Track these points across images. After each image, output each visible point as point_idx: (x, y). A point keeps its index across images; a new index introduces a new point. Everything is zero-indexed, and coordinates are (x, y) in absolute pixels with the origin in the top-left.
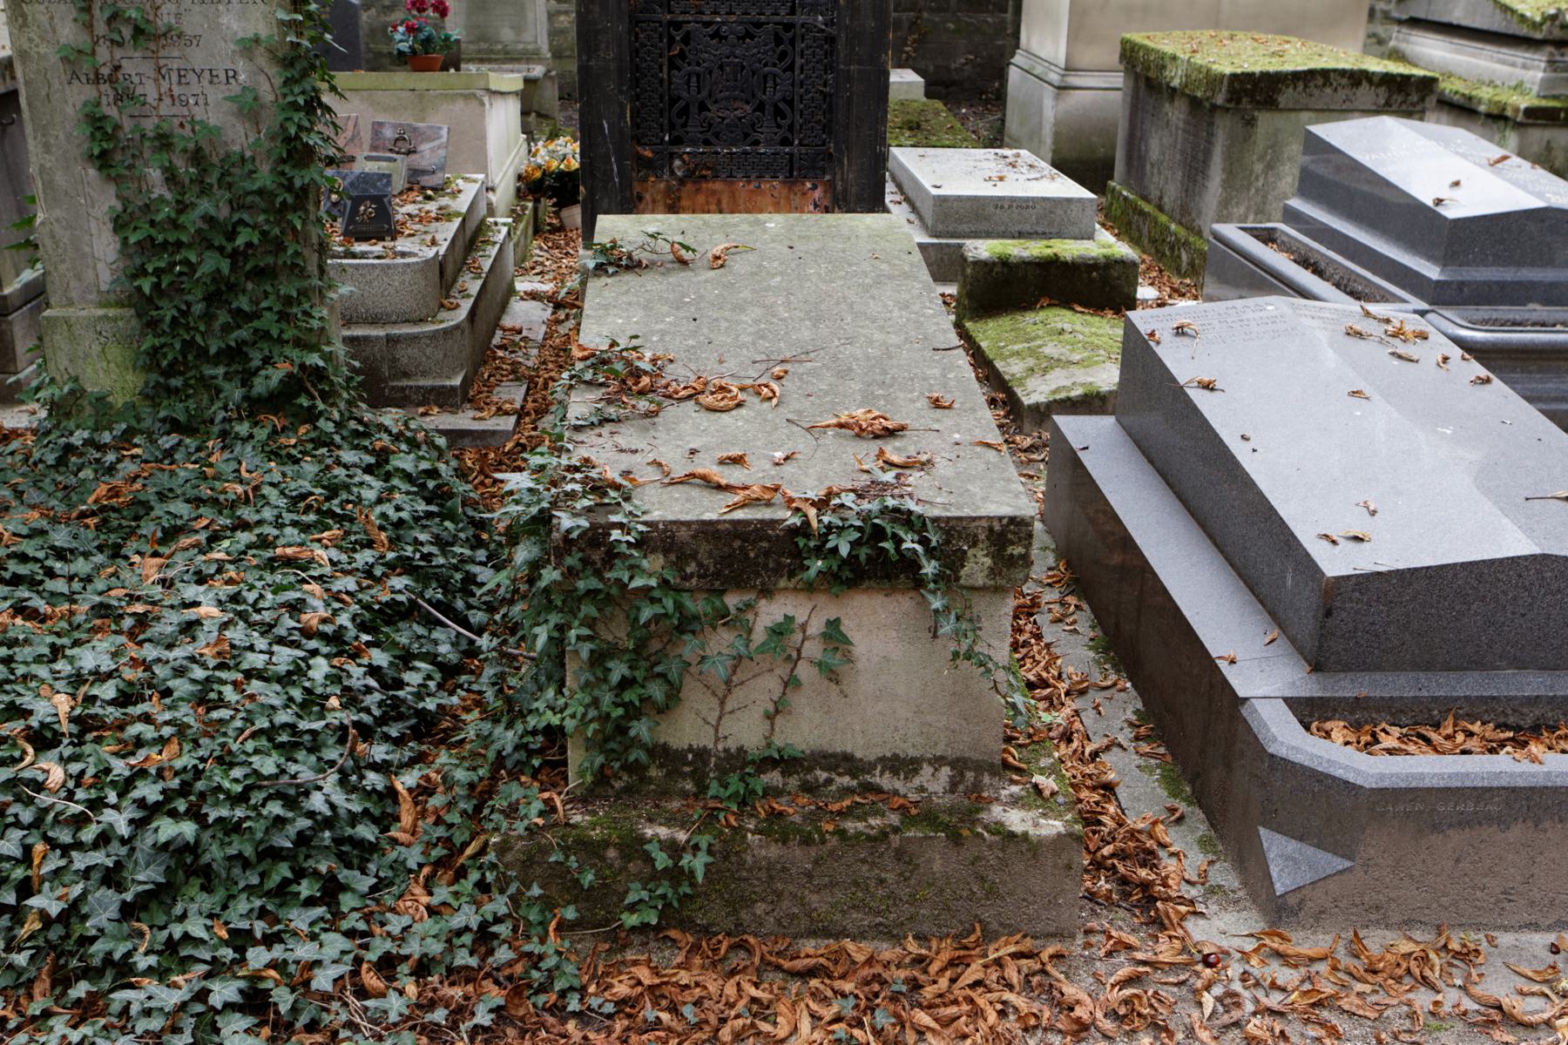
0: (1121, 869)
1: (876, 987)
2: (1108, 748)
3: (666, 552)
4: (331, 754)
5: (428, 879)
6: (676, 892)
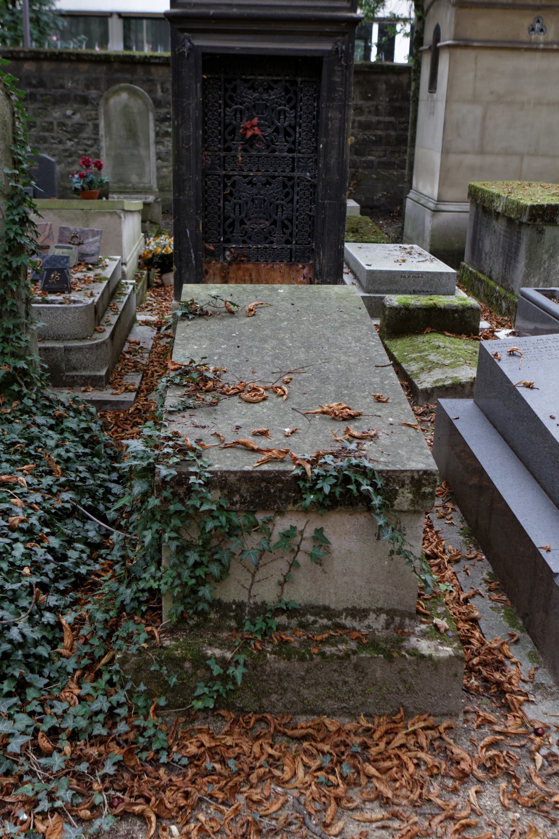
0: (484, 673)
1: (343, 748)
2: (473, 596)
3: (222, 489)
4: (24, 603)
5: (78, 678)
6: (225, 688)
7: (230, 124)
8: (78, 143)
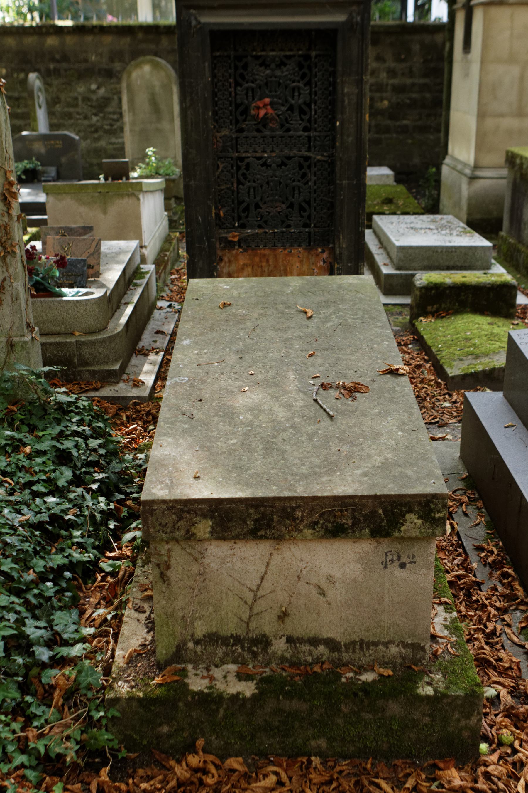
7: (242, 103)
8: (104, 118)
